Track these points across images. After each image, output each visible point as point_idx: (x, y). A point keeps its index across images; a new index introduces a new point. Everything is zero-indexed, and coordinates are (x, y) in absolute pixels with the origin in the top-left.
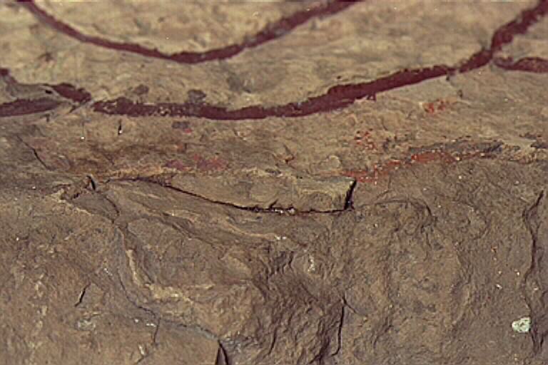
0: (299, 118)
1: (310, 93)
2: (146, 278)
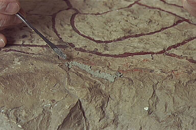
0: (115, 58)
1: (120, 53)
2: (68, 84)
